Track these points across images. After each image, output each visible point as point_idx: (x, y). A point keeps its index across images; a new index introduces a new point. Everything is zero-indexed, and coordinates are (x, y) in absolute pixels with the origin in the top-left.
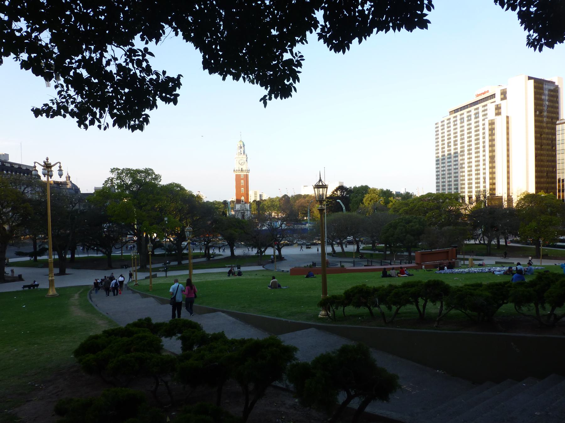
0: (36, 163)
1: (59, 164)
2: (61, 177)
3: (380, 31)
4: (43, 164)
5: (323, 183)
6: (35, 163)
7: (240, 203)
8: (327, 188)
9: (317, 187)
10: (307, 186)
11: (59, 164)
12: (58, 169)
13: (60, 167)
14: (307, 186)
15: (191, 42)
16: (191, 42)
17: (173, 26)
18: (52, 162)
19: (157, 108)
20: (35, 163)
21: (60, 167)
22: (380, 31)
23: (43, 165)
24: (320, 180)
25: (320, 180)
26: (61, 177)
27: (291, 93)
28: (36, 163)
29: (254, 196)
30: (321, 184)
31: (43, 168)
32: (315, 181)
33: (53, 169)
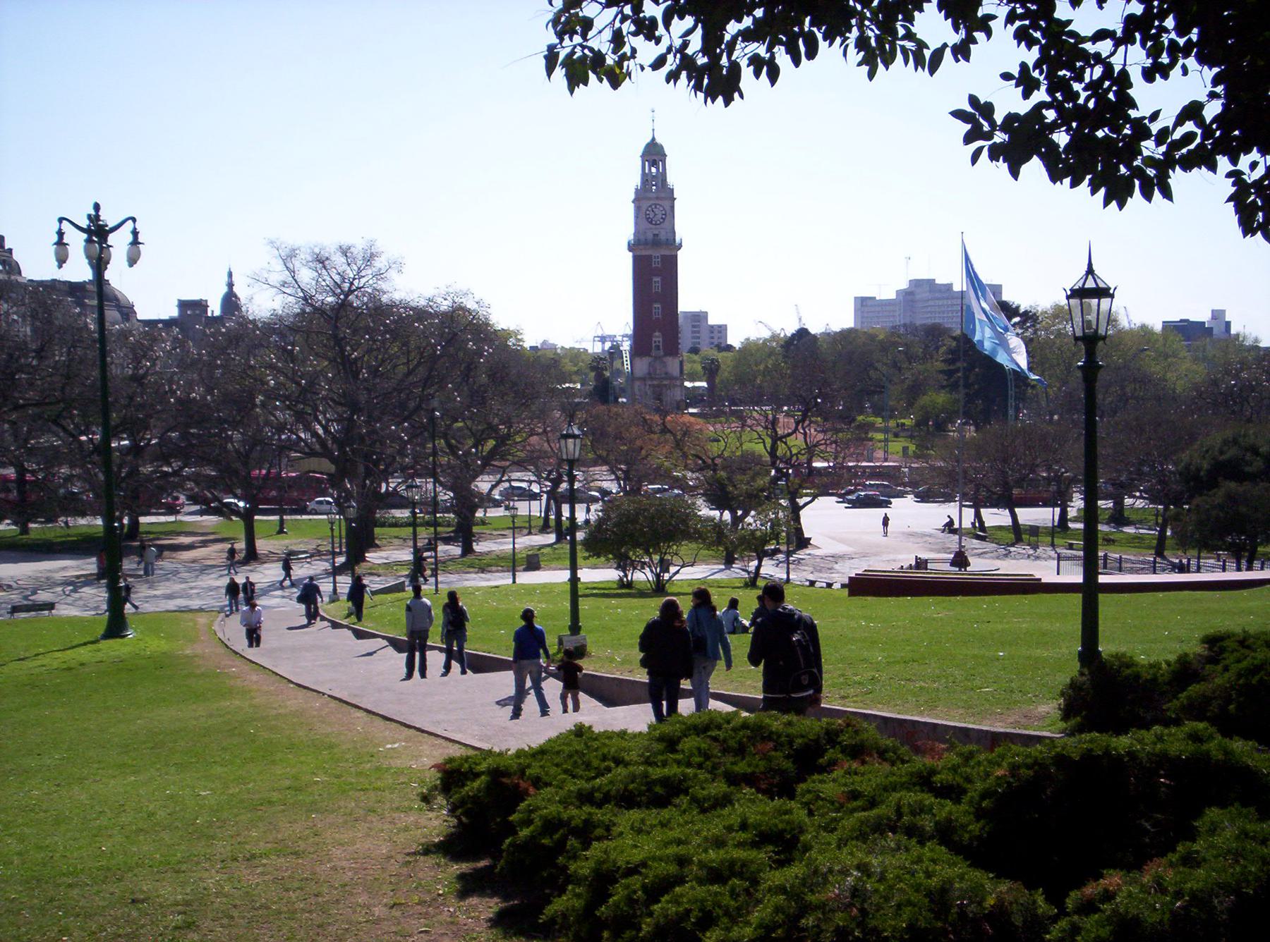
0: (64, 222)
1: (130, 222)
2: (60, 267)
3: (642, 654)
4: (84, 223)
5: (1098, 281)
6: (61, 220)
7: (650, 356)
8: (1112, 296)
9: (1079, 293)
10: (230, 275)
11: (130, 222)
12: (130, 238)
13: (135, 233)
14: (230, 275)
15: (1102, 191)
16: (1102, 191)
17: (1261, 544)
18: (109, 218)
19: (742, 96)
20: (61, 220)
21: (135, 233)
22: (642, 654)
23: (85, 227)
24: (1090, 271)
25: (1090, 271)
26: (60, 267)
27: (1171, 171)
28: (64, 222)
29: (690, 328)
30: (1090, 284)
31: (85, 236)
32: (1074, 277)
33: (112, 239)
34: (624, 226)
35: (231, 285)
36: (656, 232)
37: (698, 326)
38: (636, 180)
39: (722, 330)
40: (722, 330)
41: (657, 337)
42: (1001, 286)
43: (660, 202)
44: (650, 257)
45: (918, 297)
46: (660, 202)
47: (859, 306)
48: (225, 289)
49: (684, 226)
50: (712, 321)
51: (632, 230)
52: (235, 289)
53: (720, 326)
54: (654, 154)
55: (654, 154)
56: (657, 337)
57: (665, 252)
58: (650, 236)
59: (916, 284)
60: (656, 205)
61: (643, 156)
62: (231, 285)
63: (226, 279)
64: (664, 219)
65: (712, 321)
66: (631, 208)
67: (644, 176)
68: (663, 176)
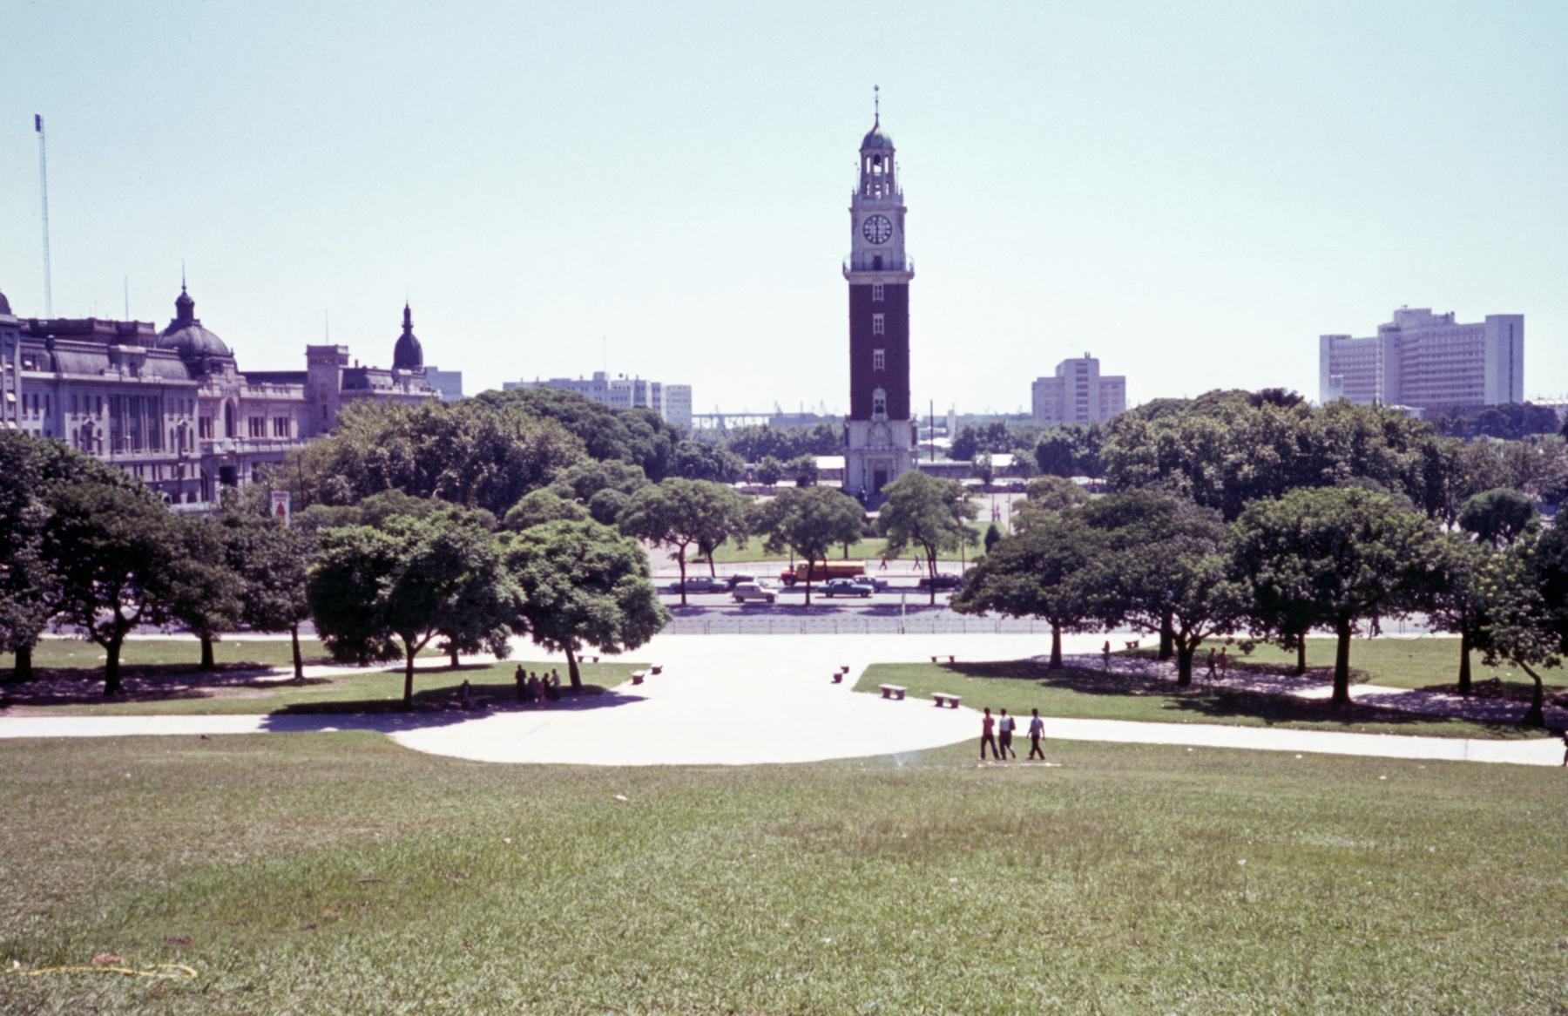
10: (407, 313)
14: (407, 313)
34: (839, 245)
35: (407, 326)
36: (877, 253)
37: (1078, 379)
38: (854, 182)
39: (1118, 383)
40: (1118, 383)
41: (879, 395)
42: (1322, 338)
43: (885, 213)
44: (869, 287)
45: (1405, 333)
46: (885, 213)
47: (1327, 349)
48: (401, 332)
49: (918, 247)
50: (1105, 371)
51: (847, 248)
52: (414, 332)
53: (685, 387)
54: (876, 148)
55: (876, 148)
56: (879, 395)
57: (890, 279)
58: (869, 260)
59: (1405, 314)
60: (877, 216)
61: (862, 150)
62: (407, 326)
63: (401, 318)
64: (889, 236)
65: (1105, 371)
66: (847, 219)
67: (864, 175)
68: (890, 178)
